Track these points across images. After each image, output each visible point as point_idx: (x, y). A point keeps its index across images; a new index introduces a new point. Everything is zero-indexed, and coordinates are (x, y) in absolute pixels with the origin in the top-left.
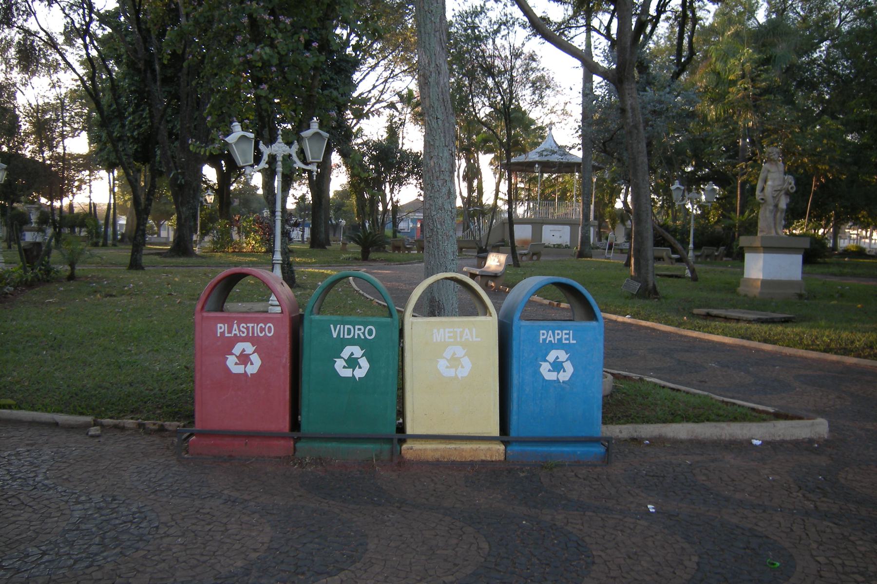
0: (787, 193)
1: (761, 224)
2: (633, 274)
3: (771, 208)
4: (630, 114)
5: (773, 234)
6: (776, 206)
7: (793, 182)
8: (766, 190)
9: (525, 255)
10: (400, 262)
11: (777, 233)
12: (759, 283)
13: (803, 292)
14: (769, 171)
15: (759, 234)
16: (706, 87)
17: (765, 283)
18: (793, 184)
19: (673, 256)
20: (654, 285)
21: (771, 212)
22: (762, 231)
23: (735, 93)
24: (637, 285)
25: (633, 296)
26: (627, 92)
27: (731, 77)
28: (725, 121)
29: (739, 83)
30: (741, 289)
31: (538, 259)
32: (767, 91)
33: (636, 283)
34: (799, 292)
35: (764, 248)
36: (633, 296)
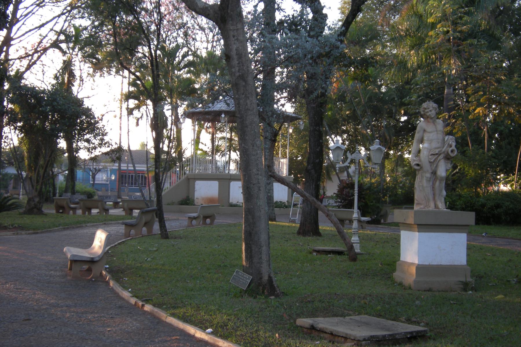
0: (447, 158)
1: (417, 196)
2: (244, 263)
3: (428, 175)
4: (235, 62)
5: (432, 207)
6: (434, 173)
7: (454, 144)
8: (421, 154)
9: (195, 218)
10: (36, 230)
11: (436, 206)
12: (413, 270)
13: (469, 279)
14: (425, 131)
15: (416, 208)
16: (407, 30)
17: (420, 268)
18: (453, 147)
19: (363, 219)
20: (270, 277)
21: (429, 180)
22: (418, 204)
23: (434, 37)
24: (248, 278)
25: (242, 293)
26: (232, 33)
27: (430, 20)
28: (428, 67)
29: (438, 26)
30: (397, 275)
31: (212, 223)
32: (471, 35)
33: (247, 276)
34: (463, 279)
35: (418, 225)
36: (242, 293)
